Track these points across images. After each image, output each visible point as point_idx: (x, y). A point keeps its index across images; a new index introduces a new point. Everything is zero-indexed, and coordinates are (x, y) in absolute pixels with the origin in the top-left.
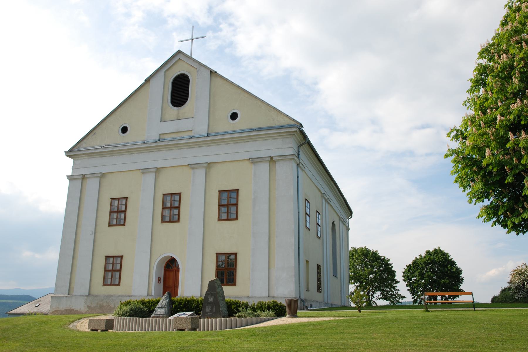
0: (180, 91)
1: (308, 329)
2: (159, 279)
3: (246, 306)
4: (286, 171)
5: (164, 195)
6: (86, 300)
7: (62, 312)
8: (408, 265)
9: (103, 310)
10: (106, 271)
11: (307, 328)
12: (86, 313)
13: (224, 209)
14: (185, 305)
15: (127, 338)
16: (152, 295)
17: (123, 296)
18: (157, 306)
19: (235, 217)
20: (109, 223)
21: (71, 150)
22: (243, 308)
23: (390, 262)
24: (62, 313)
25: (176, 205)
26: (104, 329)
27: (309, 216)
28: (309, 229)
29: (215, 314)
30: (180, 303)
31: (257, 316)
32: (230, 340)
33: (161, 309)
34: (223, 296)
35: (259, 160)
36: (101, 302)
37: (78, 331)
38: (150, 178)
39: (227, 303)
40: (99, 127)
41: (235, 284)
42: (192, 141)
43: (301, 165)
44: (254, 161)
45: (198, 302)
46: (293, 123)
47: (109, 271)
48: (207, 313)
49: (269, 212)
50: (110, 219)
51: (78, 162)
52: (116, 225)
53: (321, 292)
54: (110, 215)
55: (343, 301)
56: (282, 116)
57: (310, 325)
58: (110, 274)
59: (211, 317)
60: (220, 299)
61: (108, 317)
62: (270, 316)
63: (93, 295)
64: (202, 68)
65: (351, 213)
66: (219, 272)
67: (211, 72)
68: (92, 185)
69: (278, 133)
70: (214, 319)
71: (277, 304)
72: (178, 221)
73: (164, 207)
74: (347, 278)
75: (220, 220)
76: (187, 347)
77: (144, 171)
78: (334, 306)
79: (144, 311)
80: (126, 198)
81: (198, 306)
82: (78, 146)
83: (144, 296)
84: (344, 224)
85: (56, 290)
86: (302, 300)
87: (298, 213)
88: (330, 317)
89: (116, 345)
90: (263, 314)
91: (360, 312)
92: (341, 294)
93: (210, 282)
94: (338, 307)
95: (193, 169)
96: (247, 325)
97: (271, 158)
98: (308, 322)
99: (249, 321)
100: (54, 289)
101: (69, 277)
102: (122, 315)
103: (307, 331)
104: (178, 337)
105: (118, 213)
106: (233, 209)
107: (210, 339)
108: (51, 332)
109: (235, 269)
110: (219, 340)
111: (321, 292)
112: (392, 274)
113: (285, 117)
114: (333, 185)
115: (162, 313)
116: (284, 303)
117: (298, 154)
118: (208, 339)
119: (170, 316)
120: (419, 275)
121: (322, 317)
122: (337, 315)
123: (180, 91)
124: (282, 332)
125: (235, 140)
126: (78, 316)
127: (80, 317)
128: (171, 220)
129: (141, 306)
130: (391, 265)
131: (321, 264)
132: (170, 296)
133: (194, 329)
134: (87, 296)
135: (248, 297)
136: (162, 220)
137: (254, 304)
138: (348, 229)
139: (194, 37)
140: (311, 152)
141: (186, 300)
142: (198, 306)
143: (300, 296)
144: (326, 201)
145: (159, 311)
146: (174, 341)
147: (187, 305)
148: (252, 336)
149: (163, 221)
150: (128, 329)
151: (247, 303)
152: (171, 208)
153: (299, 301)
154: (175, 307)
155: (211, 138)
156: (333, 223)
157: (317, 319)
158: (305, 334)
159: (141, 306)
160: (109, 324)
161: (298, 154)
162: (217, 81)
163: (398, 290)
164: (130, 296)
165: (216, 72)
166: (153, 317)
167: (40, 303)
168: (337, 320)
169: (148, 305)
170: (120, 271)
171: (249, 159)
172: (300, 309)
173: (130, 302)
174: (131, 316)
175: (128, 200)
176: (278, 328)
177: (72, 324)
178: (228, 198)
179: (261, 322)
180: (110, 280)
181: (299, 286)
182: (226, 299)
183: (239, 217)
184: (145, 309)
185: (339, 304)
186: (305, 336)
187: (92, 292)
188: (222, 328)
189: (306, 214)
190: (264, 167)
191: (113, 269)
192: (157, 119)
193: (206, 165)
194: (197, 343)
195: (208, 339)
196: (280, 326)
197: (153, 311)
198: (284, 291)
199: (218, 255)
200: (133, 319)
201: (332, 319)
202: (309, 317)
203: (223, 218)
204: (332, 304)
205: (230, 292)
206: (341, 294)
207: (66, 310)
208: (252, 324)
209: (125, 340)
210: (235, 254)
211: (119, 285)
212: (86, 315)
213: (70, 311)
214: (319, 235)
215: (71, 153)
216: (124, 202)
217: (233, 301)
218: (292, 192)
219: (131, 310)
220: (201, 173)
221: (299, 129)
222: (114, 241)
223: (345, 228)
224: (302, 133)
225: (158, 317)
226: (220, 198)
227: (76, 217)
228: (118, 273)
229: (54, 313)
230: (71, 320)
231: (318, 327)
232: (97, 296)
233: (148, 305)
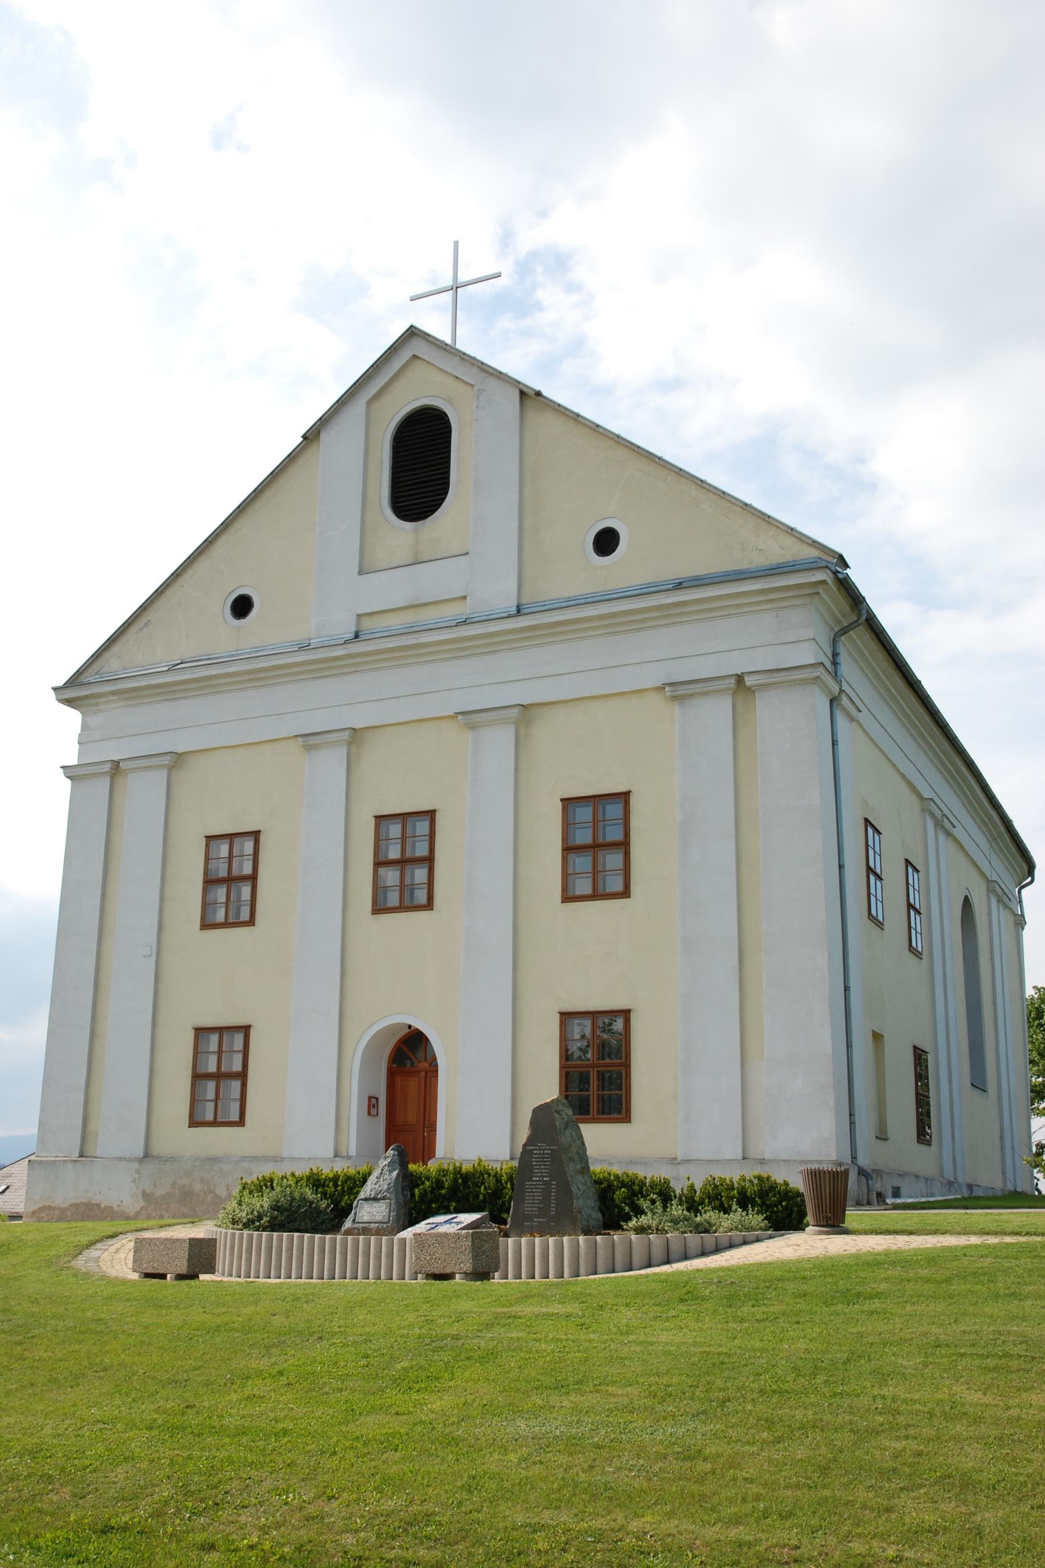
0: (420, 465)
1: (887, 1279)
2: (372, 1103)
3: (665, 1194)
4: (792, 721)
5: (379, 818)
6: (138, 1172)
7: (63, 1211)
9: (188, 1204)
10: (198, 1077)
11: (881, 1274)
12: (137, 1216)
13: (583, 862)
14: (454, 1189)
15: (256, 1303)
16: (348, 1157)
17: (255, 1159)
18: (362, 1195)
19: (619, 887)
20: (203, 918)
21: (75, 681)
22: (653, 1202)
24: (62, 1215)
25: (422, 850)
26: (184, 1270)
27: (879, 877)
28: (880, 925)
29: (556, 1219)
30: (439, 1184)
31: (705, 1229)
32: (606, 1314)
33: (376, 1205)
34: (584, 1159)
35: (698, 688)
36: (186, 1181)
37: (104, 1277)
38: (331, 764)
39: (599, 1182)
41: (627, 1119)
42: (470, 634)
43: (845, 700)
44: (679, 692)
45: (498, 1180)
46: (814, 553)
48: (530, 1218)
50: (205, 905)
51: (96, 720)
52: (226, 925)
53: (929, 1143)
55: (1009, 1174)
56: (773, 531)
57: (893, 1263)
58: (211, 1085)
59: (544, 1231)
60: (572, 1168)
61: (200, 1231)
62: (751, 1229)
64: (493, 383)
65: (1029, 867)
66: (573, 1076)
67: (523, 394)
68: (145, 792)
69: (760, 592)
70: (551, 1240)
71: (773, 1187)
72: (429, 906)
73: (382, 858)
74: (1022, 1095)
75: (568, 897)
76: (456, 1338)
78: (977, 1192)
79: (317, 1208)
80: (256, 835)
81: (497, 1193)
82: (95, 667)
83: (325, 1160)
84: (1006, 906)
85: (41, 1139)
86: (861, 1172)
87: (841, 867)
88: (965, 1232)
89: (218, 1329)
90: (726, 1222)
92: (1002, 1149)
93: (536, 1111)
94: (994, 1198)
95: (473, 727)
96: (668, 1262)
97: (740, 679)
98: (887, 1253)
99: (676, 1248)
100: (36, 1138)
101: (82, 1098)
102: (246, 1226)
103: (883, 1287)
104: (427, 1300)
105: (231, 884)
106: (613, 860)
107: (537, 1310)
108: (16, 1279)
109: (627, 1065)
110: (568, 1316)
111: (929, 1143)
114: (964, 769)
115: (379, 1218)
116: (797, 1183)
117: (835, 663)
118: (527, 1309)
119: (404, 1228)
121: (935, 1232)
122: (993, 1227)
123: (420, 465)
124: (790, 1286)
126: (106, 1227)
127: (113, 1230)
128: (407, 903)
129: (309, 1193)
131: (926, 1045)
132: (402, 1160)
133: (481, 1275)
134: (140, 1160)
135: (673, 1161)
136: (375, 902)
137: (692, 1188)
138: (1020, 922)
139: (463, 277)
140: (881, 656)
141: (458, 1172)
142: (497, 1193)
143: (854, 1158)
144: (938, 824)
145: (369, 1211)
146: (411, 1317)
147: (462, 1190)
148: (682, 1300)
149: (379, 908)
150: (259, 1274)
151: (667, 1182)
152: (402, 862)
153: (853, 1176)
154: (419, 1200)
155: (530, 619)
156: (967, 903)
157: (917, 1242)
158: (878, 1295)
159: (309, 1193)
160: (202, 1257)
161: (835, 663)
162: (537, 418)
164: (278, 1159)
165: (538, 394)
166: (348, 1232)
167: (9, 1181)
168: (994, 1247)
169: (331, 1189)
170: (243, 1076)
171: (662, 688)
172: (858, 1204)
173: (272, 1180)
174: (274, 1226)
175: (262, 838)
176: (778, 1273)
177: (86, 1253)
178: (595, 822)
179: (718, 1250)
180: (210, 1106)
181: (852, 1123)
182: (595, 1168)
183: (634, 888)
184: (323, 1204)
185: (998, 1184)
186: (876, 1304)
188: (582, 1270)
189: (869, 870)
190: (718, 711)
191: (220, 1071)
192: (350, 561)
193: (516, 711)
194: (489, 1326)
195: (527, 1309)
196: (783, 1264)
197: (346, 1211)
198: (800, 1140)
199: (566, 1017)
200: (280, 1240)
201: (974, 1240)
202: (888, 1232)
203: (578, 892)
204: (970, 1187)
205: (605, 1145)
206: (1002, 1149)
207: (76, 1206)
208: (686, 1257)
209: (250, 1309)
210: (626, 1014)
212: (135, 1225)
213: (89, 1211)
214: (917, 943)
215: (74, 691)
216: (249, 846)
217: (617, 1177)
218: (817, 794)
219: (275, 1207)
220: (500, 740)
221: (836, 573)
222: (219, 978)
223: (1011, 919)
224: (847, 587)
225: (366, 1231)
226: (567, 825)
228: (236, 1085)
229: (37, 1214)
230: (84, 1240)
231: (924, 1272)
233: (331, 1189)
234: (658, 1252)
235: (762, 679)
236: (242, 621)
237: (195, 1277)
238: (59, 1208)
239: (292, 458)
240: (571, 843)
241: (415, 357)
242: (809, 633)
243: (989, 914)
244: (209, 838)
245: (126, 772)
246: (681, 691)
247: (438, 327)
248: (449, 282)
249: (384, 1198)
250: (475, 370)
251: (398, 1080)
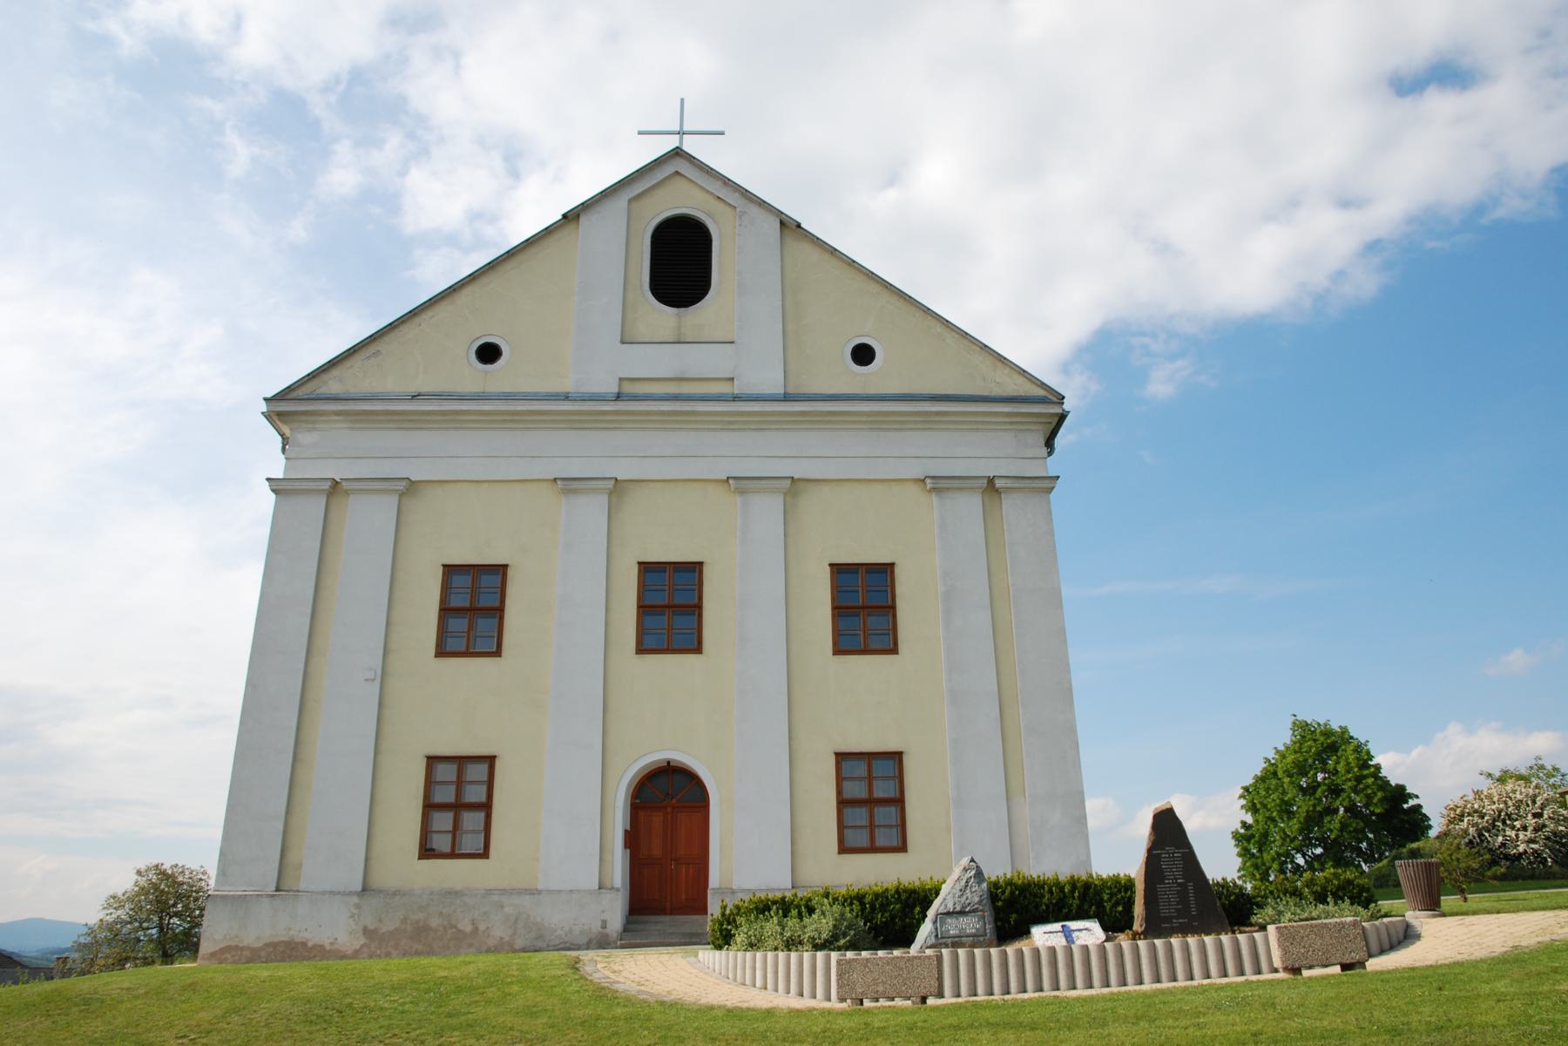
0: (680, 262)
6: (357, 906)
10: (429, 807)
12: (356, 954)
35: (956, 483)
36: (421, 916)
38: (592, 510)
40: (392, 335)
44: (938, 485)
45: (1062, 889)
56: (1007, 370)
59: (1185, 931)
64: (754, 210)
67: (782, 223)
68: (369, 519)
77: (569, 485)
91: (1465, 900)
95: (742, 492)
97: (991, 481)
101: (281, 827)
105: (473, 608)
113: (1016, 376)
123: (680, 262)
125: (877, 423)
155: (795, 405)
165: (799, 226)
187: (378, 880)
191: (459, 801)
207: (275, 945)
211: (485, 854)
222: (459, 705)
235: (1009, 483)
236: (488, 367)
238: (248, 948)
239: (548, 231)
241: (677, 173)
245: (347, 493)
249: (974, 911)
250: (737, 195)
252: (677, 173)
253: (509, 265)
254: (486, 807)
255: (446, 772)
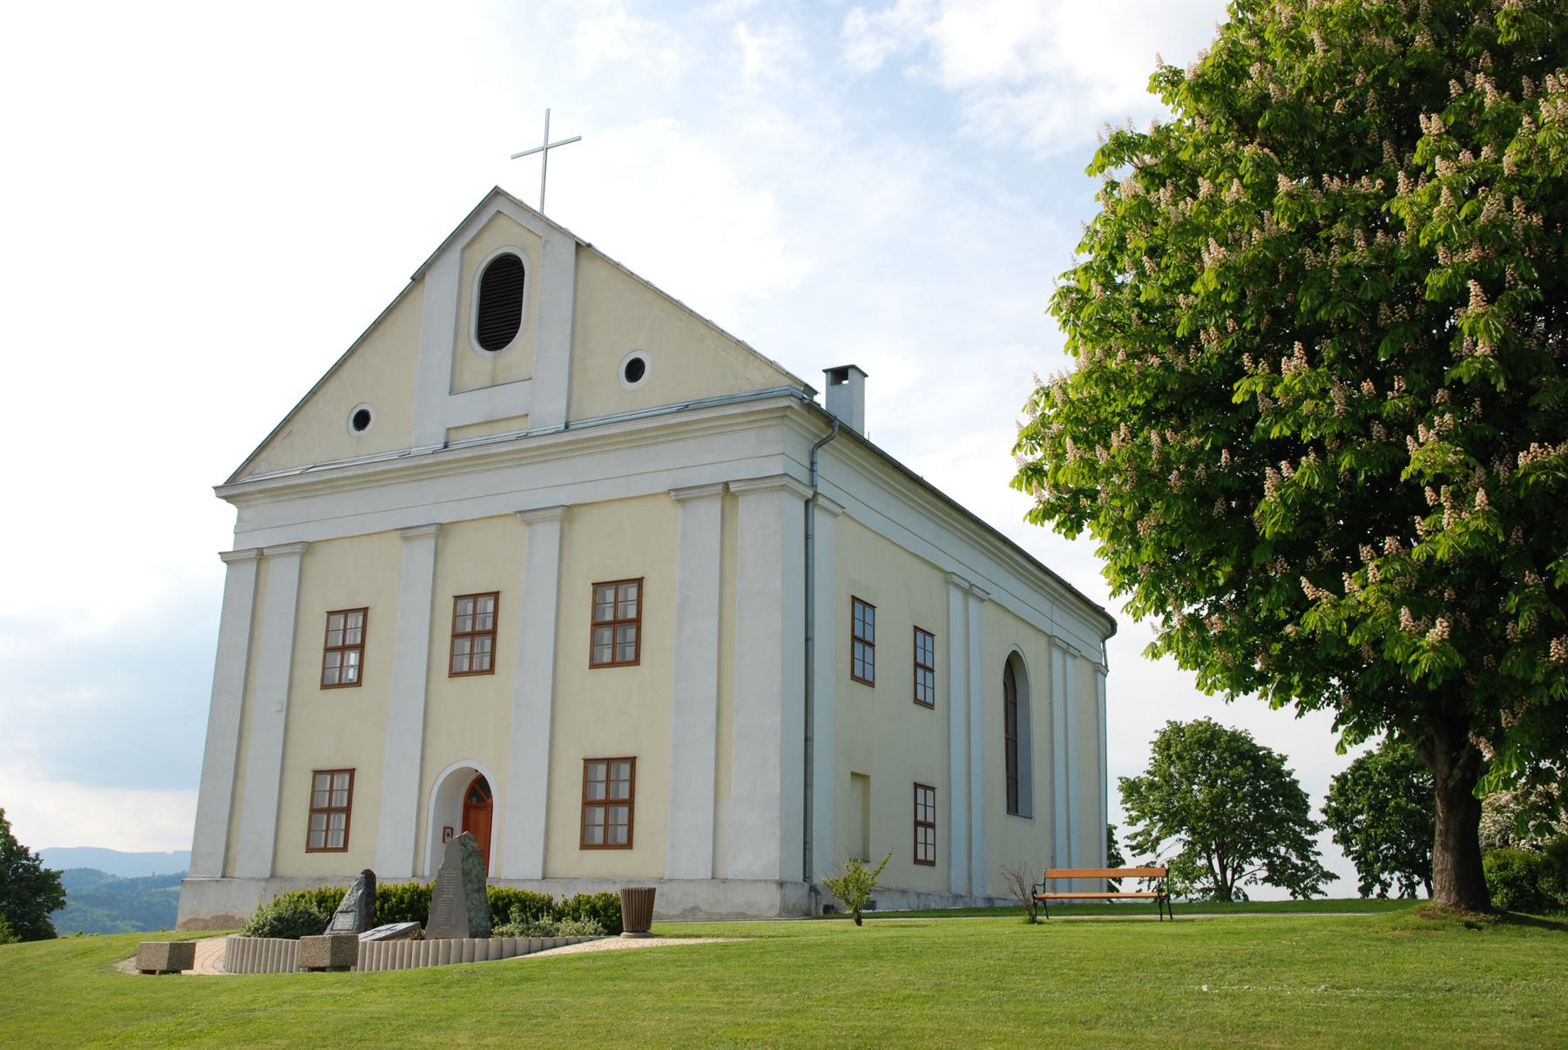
0: (500, 303)
2: (447, 832)
8: (1337, 774)
10: (314, 811)
20: (591, 658)
21: (233, 480)
23: (1286, 767)
35: (694, 493)
38: (423, 551)
40: (299, 416)
42: (531, 449)
44: (682, 496)
47: (321, 811)
49: (720, 639)
54: (593, 633)
63: (281, 878)
68: (282, 573)
69: (743, 414)
75: (595, 665)
82: (249, 469)
91: (859, 923)
97: (726, 485)
99: (507, 948)
101: (225, 828)
105: (346, 643)
112: (1296, 800)
120: (1371, 807)
123: (500, 303)
125: (635, 440)
128: (618, 659)
130: (1289, 774)
134: (266, 880)
142: (411, 903)
155: (576, 436)
159: (315, 910)
163: (1319, 854)
165: (589, 246)
175: (646, 585)
190: (710, 511)
191: (332, 807)
192: (442, 386)
193: (559, 512)
201: (711, 941)
207: (217, 918)
215: (232, 490)
223: (1088, 668)
227: (244, 666)
228: (624, 811)
232: (292, 879)
234: (492, 951)
235: (742, 486)
236: (369, 427)
237: (177, 971)
240: (599, 620)
241: (499, 212)
242: (778, 448)
243: (1050, 665)
244: (330, 613)
246: (683, 495)
247: (524, 189)
248: (541, 144)
251: (472, 812)
252: (499, 212)
253: (377, 334)
254: (630, 803)
255: (601, 771)
